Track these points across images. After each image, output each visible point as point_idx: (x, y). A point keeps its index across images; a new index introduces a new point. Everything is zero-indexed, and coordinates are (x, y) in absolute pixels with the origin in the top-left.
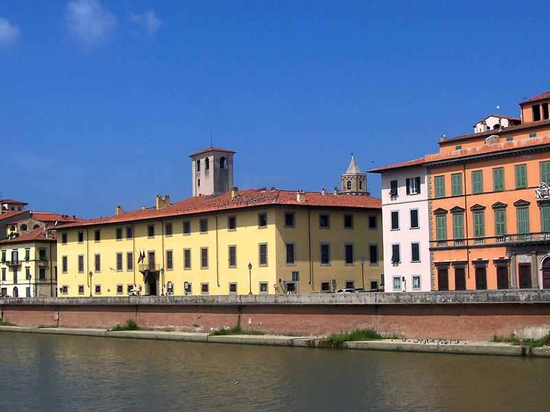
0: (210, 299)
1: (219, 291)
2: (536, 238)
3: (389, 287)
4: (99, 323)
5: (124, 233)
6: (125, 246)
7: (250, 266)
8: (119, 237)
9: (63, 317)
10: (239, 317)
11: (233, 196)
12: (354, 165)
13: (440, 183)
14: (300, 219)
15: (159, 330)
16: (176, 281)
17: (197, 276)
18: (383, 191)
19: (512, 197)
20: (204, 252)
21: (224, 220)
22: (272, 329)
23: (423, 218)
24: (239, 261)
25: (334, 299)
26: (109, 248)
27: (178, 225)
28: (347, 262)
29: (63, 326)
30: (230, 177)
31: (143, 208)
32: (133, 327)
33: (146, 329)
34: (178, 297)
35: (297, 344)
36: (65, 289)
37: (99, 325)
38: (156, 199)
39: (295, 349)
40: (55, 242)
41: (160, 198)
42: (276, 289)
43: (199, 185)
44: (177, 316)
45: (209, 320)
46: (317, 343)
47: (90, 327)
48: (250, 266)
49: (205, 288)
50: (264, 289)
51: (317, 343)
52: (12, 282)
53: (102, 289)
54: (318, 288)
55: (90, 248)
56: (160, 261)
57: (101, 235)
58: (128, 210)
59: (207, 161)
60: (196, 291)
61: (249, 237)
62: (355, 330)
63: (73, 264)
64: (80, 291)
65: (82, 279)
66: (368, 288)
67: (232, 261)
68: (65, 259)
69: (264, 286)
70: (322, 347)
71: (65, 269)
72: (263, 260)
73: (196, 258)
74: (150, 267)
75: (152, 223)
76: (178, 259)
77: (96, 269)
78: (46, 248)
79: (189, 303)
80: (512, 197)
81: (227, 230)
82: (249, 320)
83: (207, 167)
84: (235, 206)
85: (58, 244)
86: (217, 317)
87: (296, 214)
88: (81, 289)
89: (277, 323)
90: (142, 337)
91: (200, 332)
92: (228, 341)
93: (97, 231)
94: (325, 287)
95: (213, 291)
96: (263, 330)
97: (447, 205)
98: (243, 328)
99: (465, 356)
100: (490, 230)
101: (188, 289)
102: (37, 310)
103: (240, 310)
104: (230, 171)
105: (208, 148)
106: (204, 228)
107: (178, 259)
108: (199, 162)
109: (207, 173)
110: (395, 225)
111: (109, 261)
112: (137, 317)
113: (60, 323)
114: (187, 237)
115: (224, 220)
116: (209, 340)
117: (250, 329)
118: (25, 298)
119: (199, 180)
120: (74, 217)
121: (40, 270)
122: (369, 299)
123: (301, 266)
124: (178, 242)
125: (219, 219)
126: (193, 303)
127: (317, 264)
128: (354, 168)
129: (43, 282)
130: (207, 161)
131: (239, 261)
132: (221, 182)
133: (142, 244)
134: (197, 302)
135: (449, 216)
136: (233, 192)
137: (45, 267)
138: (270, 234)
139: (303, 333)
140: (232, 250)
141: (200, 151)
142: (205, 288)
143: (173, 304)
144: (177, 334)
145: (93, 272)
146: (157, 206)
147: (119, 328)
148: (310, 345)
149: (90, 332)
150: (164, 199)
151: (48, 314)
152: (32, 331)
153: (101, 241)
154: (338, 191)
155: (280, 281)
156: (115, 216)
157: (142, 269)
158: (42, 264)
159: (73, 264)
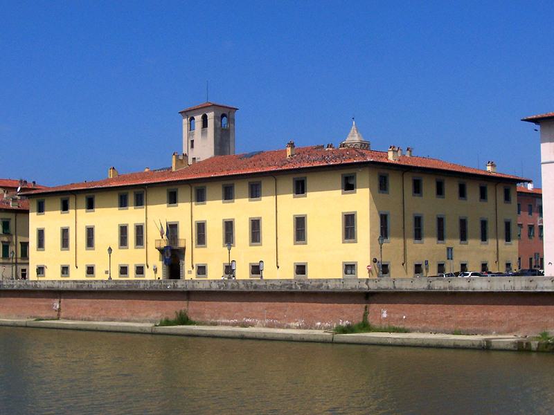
0: (313, 283)
1: (279, 272)
3: (32, 275)
4: (127, 315)
5: (131, 199)
6: (132, 216)
7: (110, 250)
8: (123, 204)
9: (66, 305)
10: (366, 307)
11: (289, 153)
12: (355, 131)
14: (394, 182)
15: (226, 324)
16: (208, 262)
17: (244, 255)
18: (542, 145)
20: (255, 225)
21: (83, 200)
22: (424, 325)
24: (323, 236)
25: (532, 285)
26: (107, 219)
27: (241, 187)
28: (462, 240)
29: (67, 319)
30: (231, 138)
31: (147, 170)
32: (183, 320)
33: (205, 324)
35: (495, 347)
36: (40, 270)
37: (125, 318)
38: (172, 158)
40: (27, 212)
41: (177, 157)
42: (370, 271)
43: (192, 146)
44: (259, 306)
46: (534, 345)
47: (112, 320)
48: (110, 250)
49: (256, 269)
50: (65, 272)
51: (534, 345)
53: (96, 270)
54: (411, 270)
55: (79, 219)
56: (186, 235)
57: (96, 203)
58: (122, 172)
59: (205, 119)
60: (242, 273)
61: (325, 205)
62: (164, 319)
63: (53, 239)
64: (63, 273)
66: (503, 270)
67: (90, 243)
68: (41, 233)
70: (543, 352)
71: (41, 245)
73: (242, 232)
74: (170, 243)
75: (174, 187)
76: (215, 233)
77: (77, 246)
78: (10, 219)
79: (277, 289)
82: (383, 312)
83: (205, 124)
84: (307, 165)
85: (30, 214)
86: (327, 308)
87: (358, 177)
88: (65, 270)
89: (433, 316)
90: (258, 336)
91: (299, 328)
92: (371, 342)
93: (91, 198)
94: (418, 269)
95: (100, 275)
96: (408, 327)
98: (371, 320)
101: (229, 270)
102: (24, 297)
104: (231, 131)
105: (203, 102)
106: (255, 193)
107: (215, 233)
108: (192, 119)
109: (204, 133)
111: (107, 234)
112: (191, 307)
113: (62, 314)
114: (173, 209)
116: (335, 340)
117: (384, 325)
119: (192, 141)
120: (34, 182)
121: (3, 246)
123: (394, 243)
124: (214, 211)
125: (279, 183)
127: (410, 242)
128: (356, 135)
129: (6, 261)
130: (205, 119)
131: (323, 236)
132: (223, 141)
133: (157, 215)
134: (291, 288)
136: (289, 149)
137: (9, 242)
138: (361, 201)
139: (477, 330)
140: (90, 232)
141: (192, 107)
142: (256, 269)
143: (252, 289)
144: (258, 329)
146: (174, 165)
147: (168, 323)
148: (522, 349)
149: (131, 327)
150: (181, 158)
151: (42, 302)
152: (28, 324)
154: (410, 151)
155: (375, 261)
156: (109, 177)
157: (158, 246)
158: (5, 239)
159: (53, 239)
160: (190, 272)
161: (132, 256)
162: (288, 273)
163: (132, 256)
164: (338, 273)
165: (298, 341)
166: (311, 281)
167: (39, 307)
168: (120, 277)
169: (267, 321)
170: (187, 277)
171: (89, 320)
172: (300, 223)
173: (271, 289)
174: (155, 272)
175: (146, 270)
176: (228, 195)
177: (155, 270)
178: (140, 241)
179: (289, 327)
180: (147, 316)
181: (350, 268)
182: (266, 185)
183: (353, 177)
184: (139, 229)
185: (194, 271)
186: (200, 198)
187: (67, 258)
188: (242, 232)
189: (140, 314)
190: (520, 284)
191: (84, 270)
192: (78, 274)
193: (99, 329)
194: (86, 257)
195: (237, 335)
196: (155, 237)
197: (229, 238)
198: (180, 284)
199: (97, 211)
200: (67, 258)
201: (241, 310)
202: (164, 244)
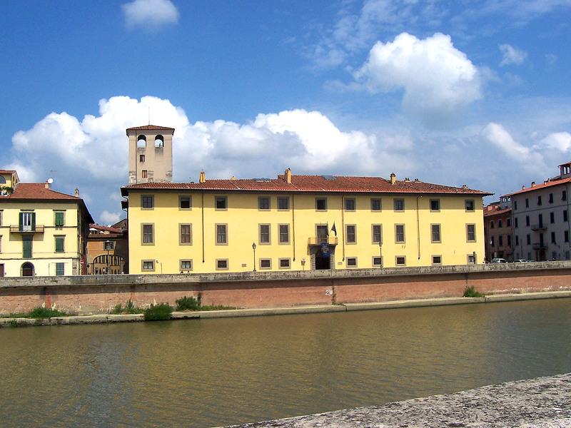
4: (413, 294)
6: (275, 217)
15: (500, 293)
17: (390, 252)
19: (3, 185)
21: (462, 202)
34: (446, 267)
37: (410, 297)
39: (202, 321)
45: (557, 281)
47: (396, 299)
60: (275, 267)
61: (454, 219)
65: (375, 250)
68: (553, 234)
73: (389, 234)
76: (364, 234)
79: (448, 272)
80: (3, 185)
81: (214, 209)
90: (388, 307)
91: (550, 290)
99: (319, 314)
101: (378, 261)
103: (332, 282)
106: (399, 206)
107: (364, 234)
121: (57, 240)
124: (363, 218)
126: (537, 268)
133: (305, 221)
145: (257, 244)
153: (383, 211)
160: (340, 263)
161: (275, 251)
162: (428, 262)
163: (275, 251)
164: (176, 269)
165: (266, 315)
166: (360, 270)
167: (306, 295)
168: (279, 269)
169: (529, 288)
170: (337, 267)
171: (370, 301)
173: (528, 269)
174: (303, 264)
175: (292, 262)
176: (376, 206)
177: (303, 263)
179: (543, 291)
180: (431, 293)
181: (472, 258)
182: (195, 199)
183: (152, 198)
185: (345, 263)
186: (350, 206)
188: (389, 234)
189: (425, 293)
192: (389, 263)
193: (433, 304)
194: (284, 251)
195: (552, 296)
201: (509, 284)
202: (313, 242)
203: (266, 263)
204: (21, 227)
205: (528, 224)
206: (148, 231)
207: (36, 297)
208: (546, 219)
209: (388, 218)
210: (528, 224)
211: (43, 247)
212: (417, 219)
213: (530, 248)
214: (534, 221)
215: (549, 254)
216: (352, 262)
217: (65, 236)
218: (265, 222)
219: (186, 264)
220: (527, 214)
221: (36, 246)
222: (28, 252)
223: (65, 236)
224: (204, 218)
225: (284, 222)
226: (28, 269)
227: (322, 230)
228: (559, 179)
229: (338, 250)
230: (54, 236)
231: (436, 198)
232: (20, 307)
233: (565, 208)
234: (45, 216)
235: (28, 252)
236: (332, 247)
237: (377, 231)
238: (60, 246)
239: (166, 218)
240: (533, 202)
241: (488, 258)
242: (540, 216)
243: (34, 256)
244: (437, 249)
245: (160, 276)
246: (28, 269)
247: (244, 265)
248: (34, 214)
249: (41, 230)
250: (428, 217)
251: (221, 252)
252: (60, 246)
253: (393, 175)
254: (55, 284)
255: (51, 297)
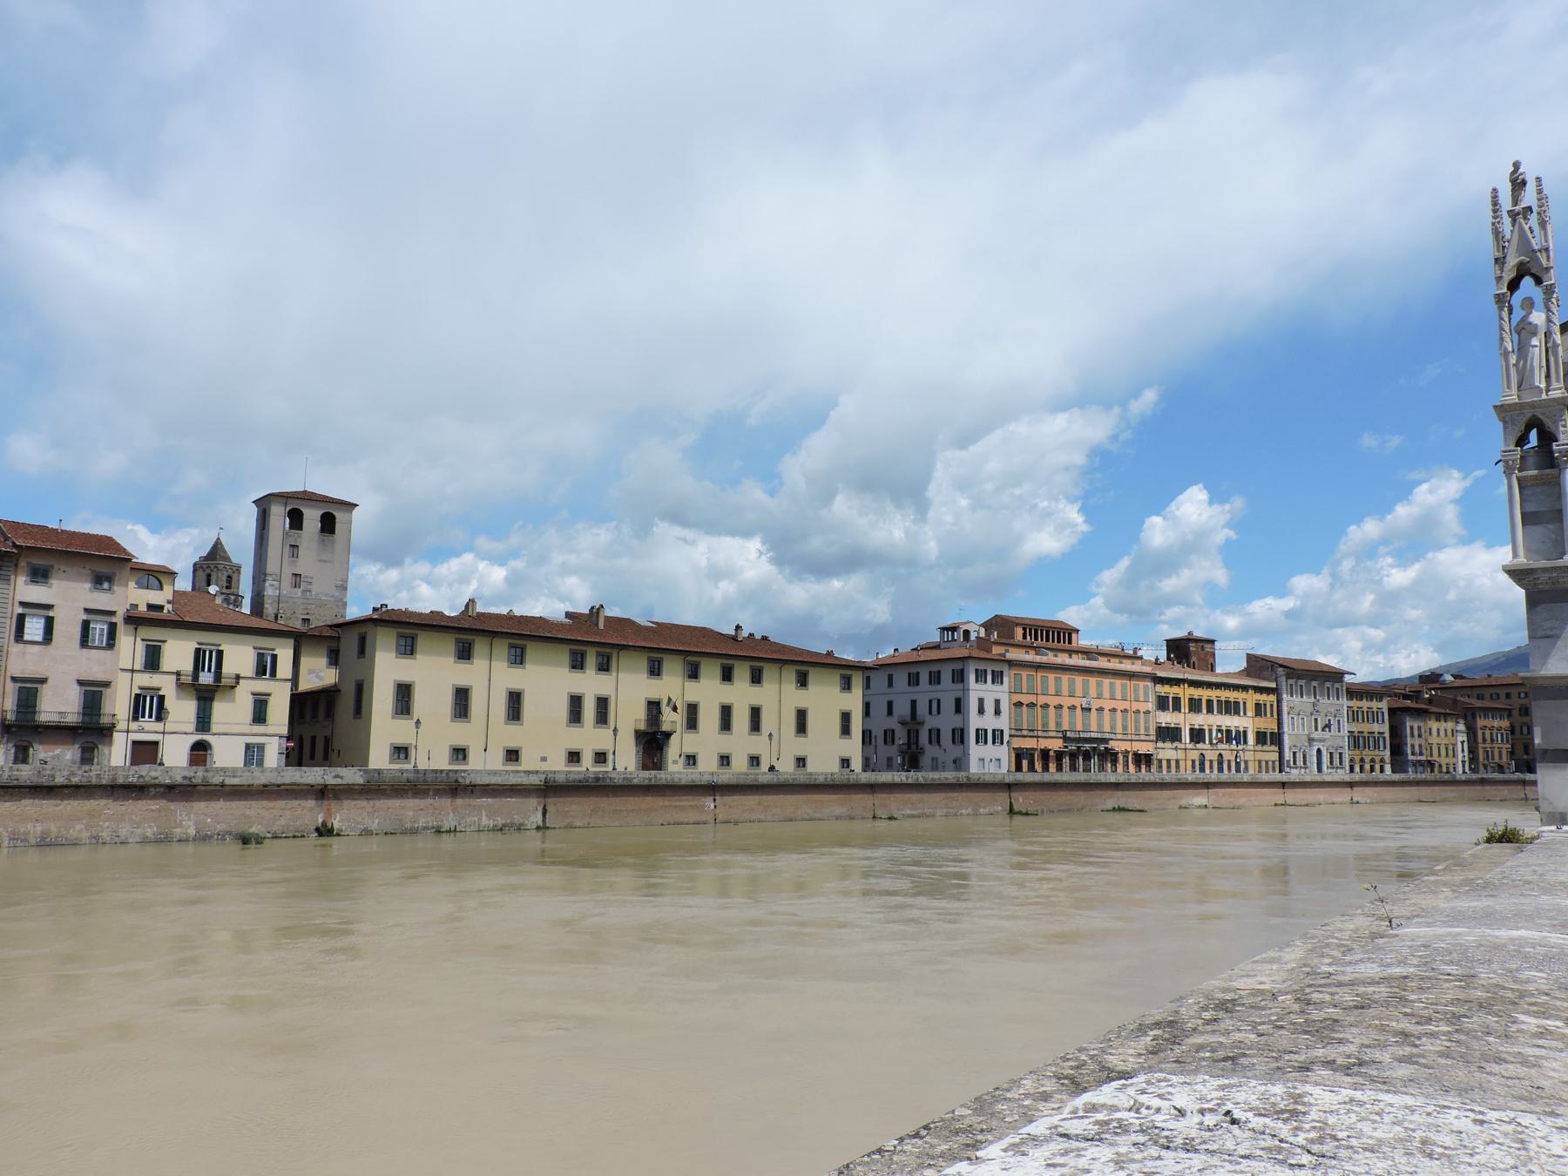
2: (1093, 735)
6: (591, 683)
8: (578, 664)
13: (1018, 677)
20: (755, 713)
23: (1004, 707)
52: (191, 727)
60: (740, 765)
61: (827, 700)
65: (793, 745)
67: (801, 728)
69: (845, 762)
72: (846, 730)
73: (741, 719)
76: (709, 718)
95: (528, 762)
97: (1026, 699)
100: (1052, 726)
101: (725, 760)
107: (709, 718)
110: (981, 711)
115: (790, 674)
118: (123, 768)
122: (949, 776)
124: (709, 692)
133: (630, 689)
135: (1119, 713)
160: (675, 762)
161: (589, 737)
163: (589, 737)
164: (834, 767)
167: (682, 808)
170: (671, 767)
172: (802, 715)
174: (626, 760)
178: (602, 716)
184: (602, 703)
185: (682, 761)
187: (725, 743)
188: (741, 719)
190: (1276, 776)
191: (501, 755)
192: (740, 765)
196: (629, 715)
197: (726, 723)
198: (662, 777)
199: (420, 657)
200: (725, 743)
202: (642, 727)
203: (574, 757)
204: (196, 676)
205: (890, 712)
206: (404, 694)
207: (310, 803)
208: (922, 709)
209: (741, 694)
210: (890, 712)
211: (231, 713)
212: (778, 696)
213: (892, 751)
214: (902, 709)
215: (925, 760)
216: (691, 759)
217: (43, 681)
218: (576, 690)
219: (460, 753)
220: (890, 698)
221: (219, 709)
222: (203, 723)
223: (43, 681)
224: (490, 675)
225: (603, 692)
226: (200, 751)
227: (654, 707)
228: (936, 647)
229: (674, 739)
230: (81, 683)
231: (805, 667)
232: (283, 822)
233: (959, 694)
234: (239, 657)
235: (203, 723)
236: (668, 735)
237: (462, 699)
238: (260, 716)
239: (434, 673)
240: (901, 679)
241: (867, 765)
242: (914, 703)
243: (214, 728)
244: (462, 734)
245: (528, 773)
246: (200, 751)
247: (544, 759)
248: (220, 654)
249: (232, 682)
250: (794, 697)
251: (511, 735)
252: (260, 716)
253: (738, 628)
254: (339, 781)
255: (334, 805)
